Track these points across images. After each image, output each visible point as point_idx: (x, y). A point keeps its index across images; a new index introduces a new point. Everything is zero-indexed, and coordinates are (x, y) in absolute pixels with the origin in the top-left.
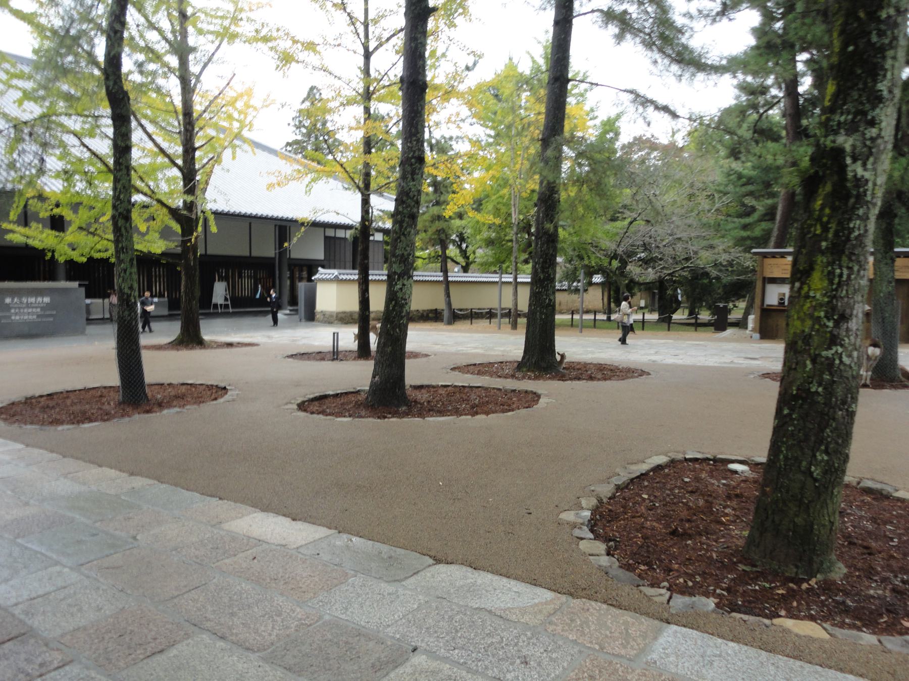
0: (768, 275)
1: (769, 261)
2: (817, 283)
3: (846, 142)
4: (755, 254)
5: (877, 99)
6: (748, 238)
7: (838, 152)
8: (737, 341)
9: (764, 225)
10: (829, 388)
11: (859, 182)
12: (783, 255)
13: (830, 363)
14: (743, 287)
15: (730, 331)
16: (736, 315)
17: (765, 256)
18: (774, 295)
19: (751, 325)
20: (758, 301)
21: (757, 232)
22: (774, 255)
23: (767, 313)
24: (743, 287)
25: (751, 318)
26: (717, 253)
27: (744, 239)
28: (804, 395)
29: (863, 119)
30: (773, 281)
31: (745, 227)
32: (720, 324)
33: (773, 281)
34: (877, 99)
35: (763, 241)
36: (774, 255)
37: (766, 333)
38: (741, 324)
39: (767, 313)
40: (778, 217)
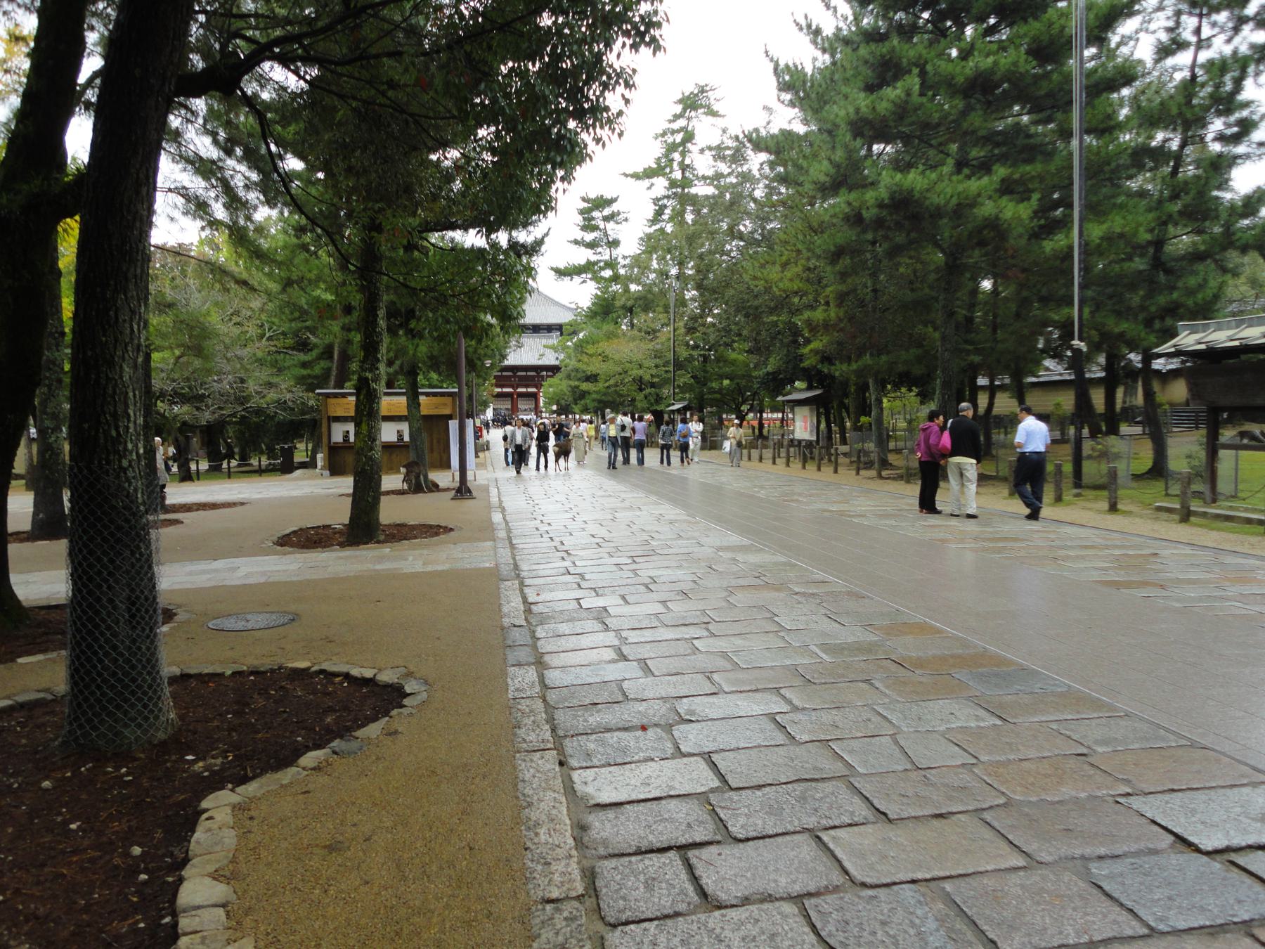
0: (332, 414)
1: (331, 401)
2: (364, 427)
3: (369, 375)
4: (319, 394)
5: (378, 360)
6: (309, 376)
7: (367, 379)
8: (309, 478)
9: (324, 364)
10: (372, 467)
11: (375, 390)
12: (344, 395)
13: (371, 458)
14: (308, 425)
15: (298, 473)
16: (299, 457)
17: (328, 396)
18: (338, 433)
19: (320, 464)
20: (325, 440)
21: (317, 370)
22: (335, 396)
23: (334, 450)
24: (308, 425)
25: (320, 456)
26: (278, 391)
27: (303, 377)
28: (363, 471)
29: (374, 368)
30: (338, 419)
31: (304, 365)
32: (287, 467)
33: (338, 419)
34: (378, 360)
35: (322, 380)
36: (335, 396)
37: (335, 469)
38: (310, 464)
39: (334, 450)
40: (336, 357)
